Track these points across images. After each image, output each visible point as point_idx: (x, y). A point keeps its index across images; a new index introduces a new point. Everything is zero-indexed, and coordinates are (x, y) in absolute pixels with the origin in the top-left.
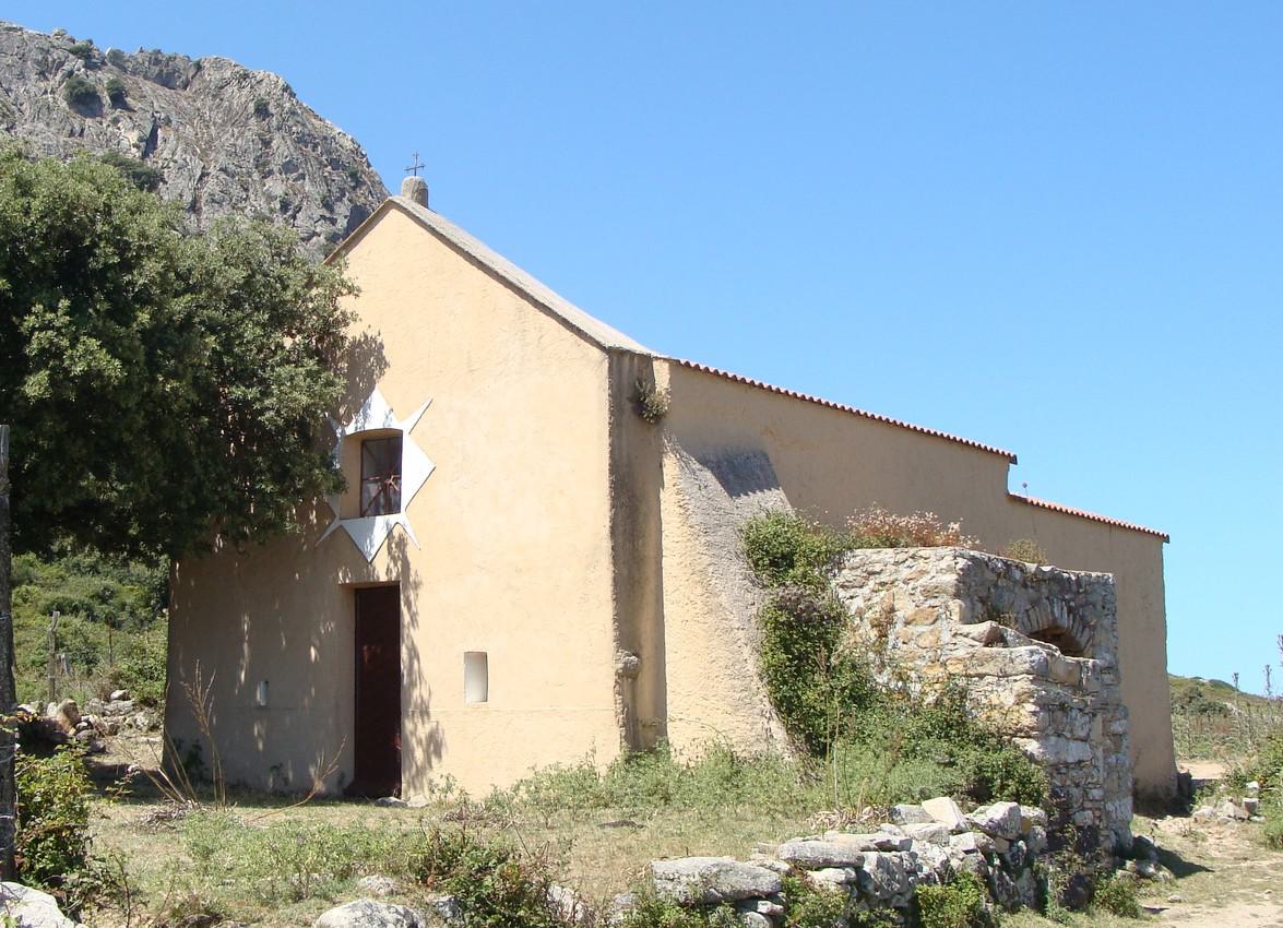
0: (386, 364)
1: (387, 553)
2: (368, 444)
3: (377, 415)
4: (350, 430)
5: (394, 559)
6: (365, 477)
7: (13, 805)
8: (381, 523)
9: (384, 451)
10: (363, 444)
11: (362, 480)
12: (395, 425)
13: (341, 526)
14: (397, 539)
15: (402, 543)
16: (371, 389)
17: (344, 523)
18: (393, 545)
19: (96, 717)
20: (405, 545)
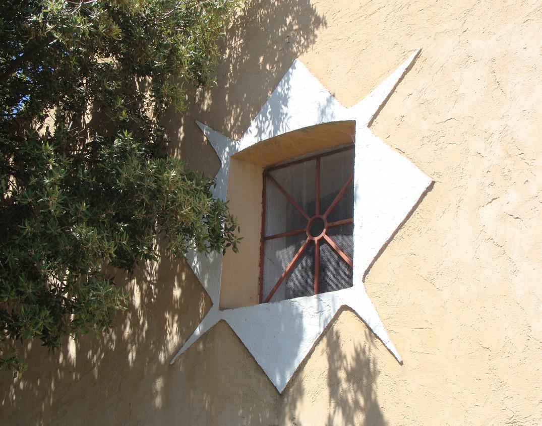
0: (320, 22)
1: (326, 391)
2: (272, 173)
3: (304, 101)
4: (247, 141)
5: (341, 403)
6: (269, 233)
7: (83, 171)
8: (312, 311)
9: (312, 191)
10: (268, 173)
11: (264, 239)
12: (339, 114)
13: (222, 321)
14: (350, 362)
15: (363, 373)
16: (288, 62)
17: (227, 315)
18: (342, 375)
19: (181, 102)
20: (372, 376)
